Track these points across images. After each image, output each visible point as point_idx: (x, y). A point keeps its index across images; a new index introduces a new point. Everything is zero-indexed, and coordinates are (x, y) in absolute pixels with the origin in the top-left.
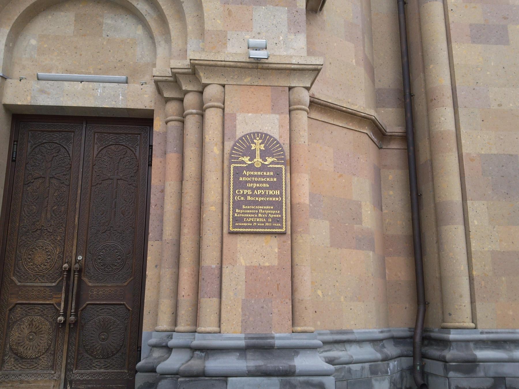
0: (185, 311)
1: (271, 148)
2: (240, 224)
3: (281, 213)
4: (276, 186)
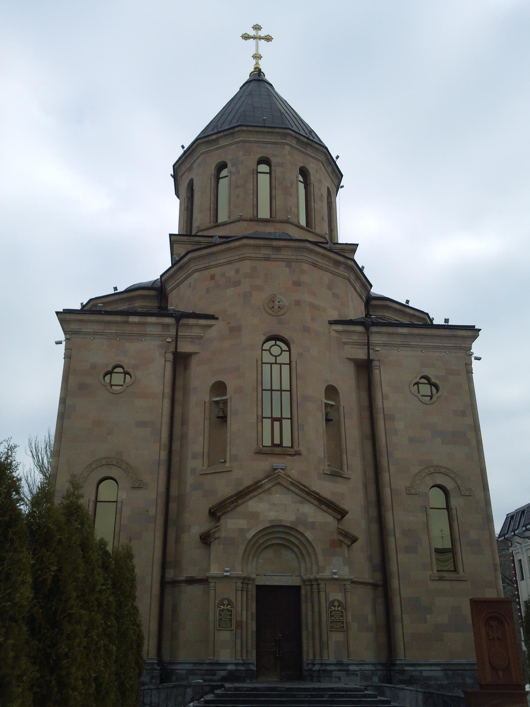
0: (318, 653)
4: (342, 616)
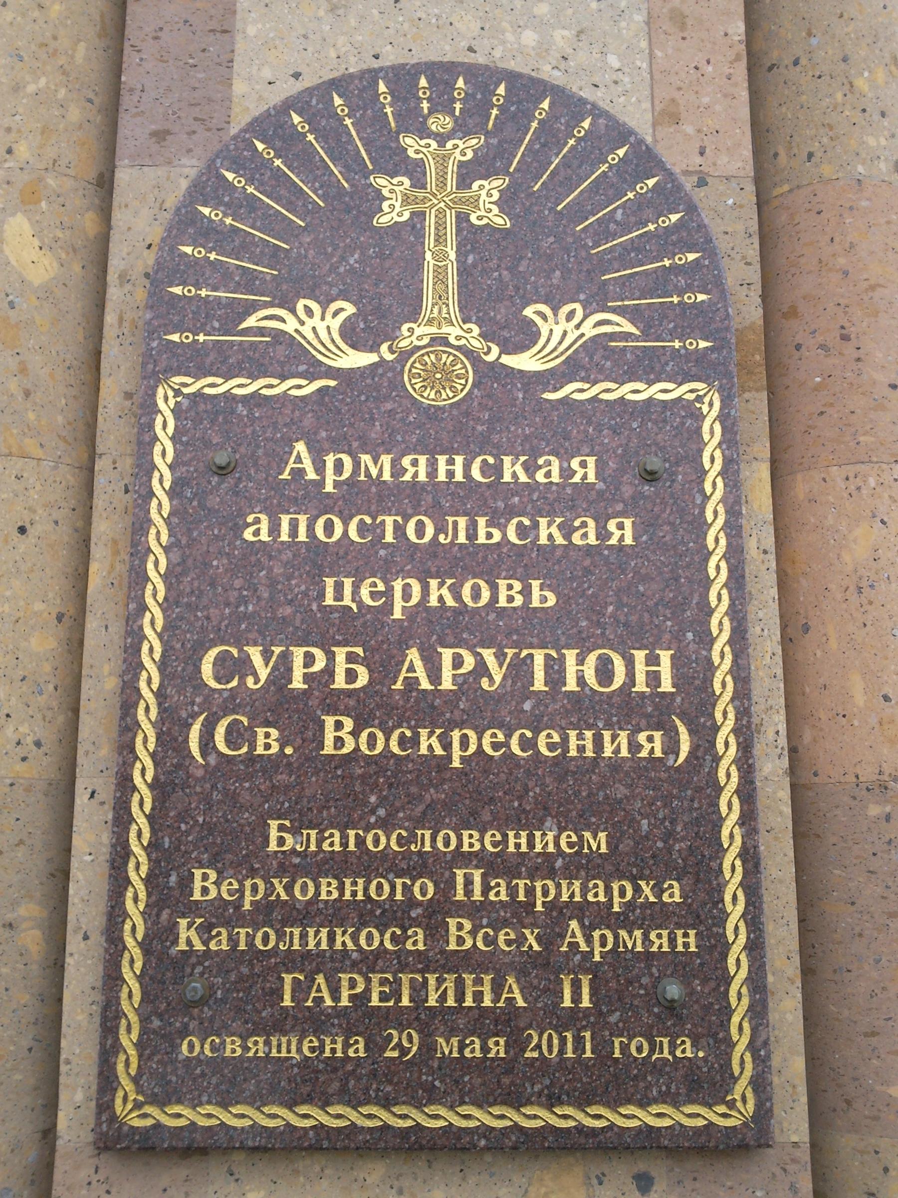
1: (578, 212)
2: (232, 1047)
3: (703, 911)
